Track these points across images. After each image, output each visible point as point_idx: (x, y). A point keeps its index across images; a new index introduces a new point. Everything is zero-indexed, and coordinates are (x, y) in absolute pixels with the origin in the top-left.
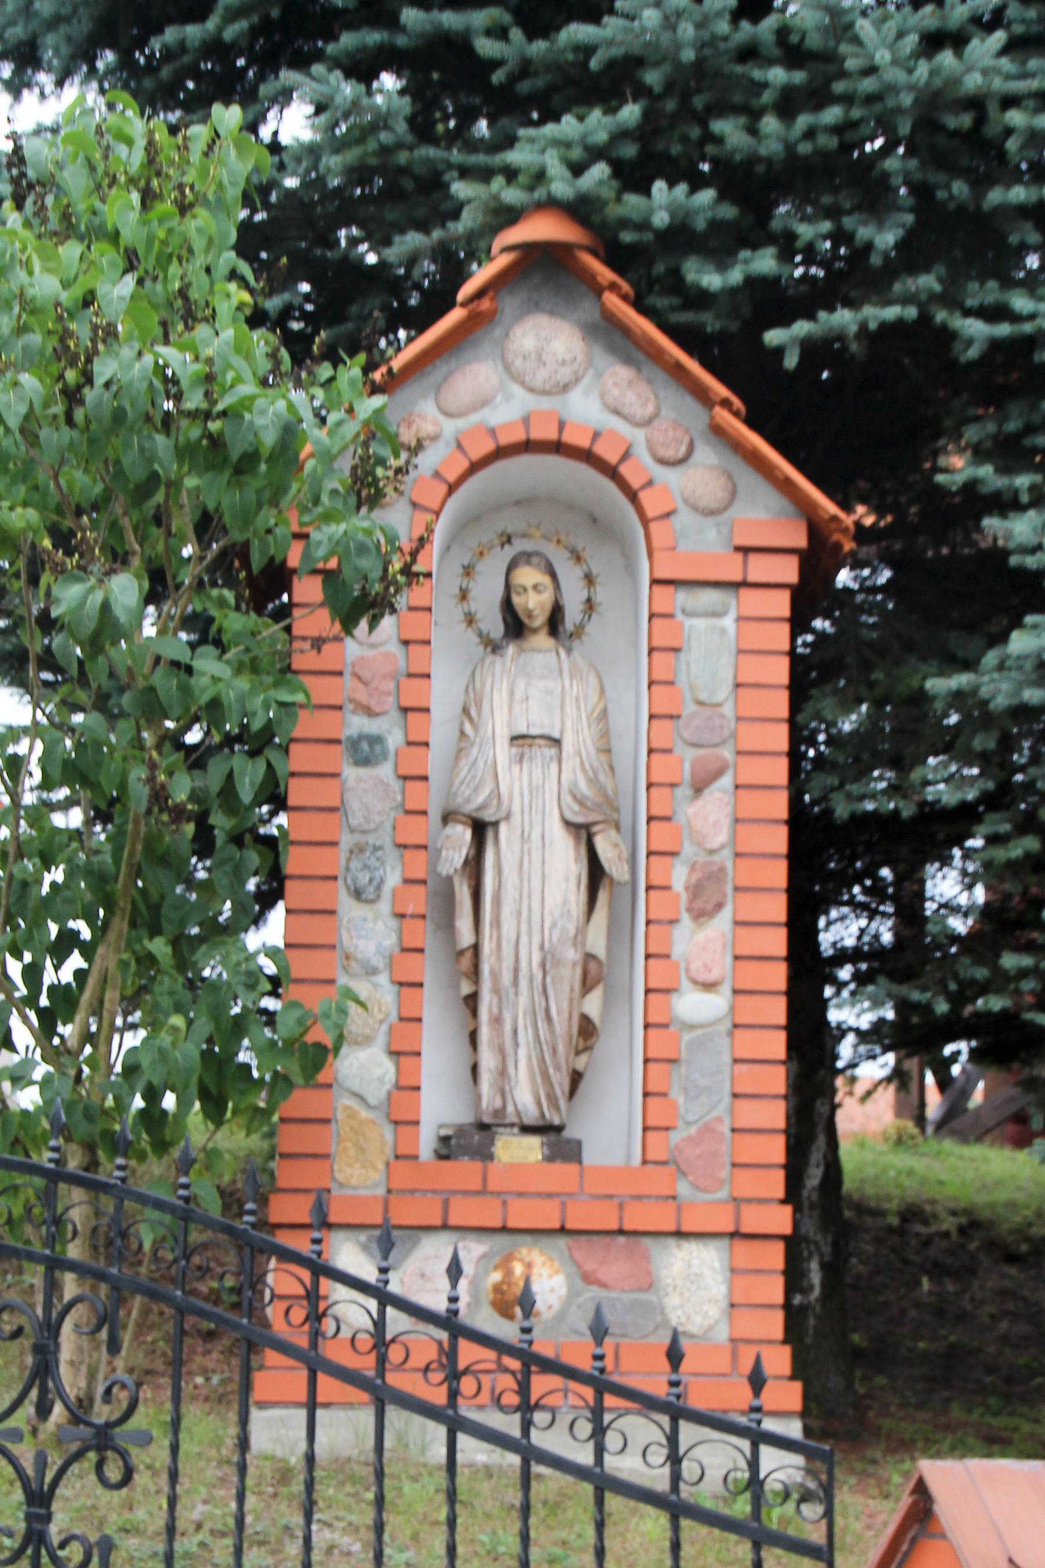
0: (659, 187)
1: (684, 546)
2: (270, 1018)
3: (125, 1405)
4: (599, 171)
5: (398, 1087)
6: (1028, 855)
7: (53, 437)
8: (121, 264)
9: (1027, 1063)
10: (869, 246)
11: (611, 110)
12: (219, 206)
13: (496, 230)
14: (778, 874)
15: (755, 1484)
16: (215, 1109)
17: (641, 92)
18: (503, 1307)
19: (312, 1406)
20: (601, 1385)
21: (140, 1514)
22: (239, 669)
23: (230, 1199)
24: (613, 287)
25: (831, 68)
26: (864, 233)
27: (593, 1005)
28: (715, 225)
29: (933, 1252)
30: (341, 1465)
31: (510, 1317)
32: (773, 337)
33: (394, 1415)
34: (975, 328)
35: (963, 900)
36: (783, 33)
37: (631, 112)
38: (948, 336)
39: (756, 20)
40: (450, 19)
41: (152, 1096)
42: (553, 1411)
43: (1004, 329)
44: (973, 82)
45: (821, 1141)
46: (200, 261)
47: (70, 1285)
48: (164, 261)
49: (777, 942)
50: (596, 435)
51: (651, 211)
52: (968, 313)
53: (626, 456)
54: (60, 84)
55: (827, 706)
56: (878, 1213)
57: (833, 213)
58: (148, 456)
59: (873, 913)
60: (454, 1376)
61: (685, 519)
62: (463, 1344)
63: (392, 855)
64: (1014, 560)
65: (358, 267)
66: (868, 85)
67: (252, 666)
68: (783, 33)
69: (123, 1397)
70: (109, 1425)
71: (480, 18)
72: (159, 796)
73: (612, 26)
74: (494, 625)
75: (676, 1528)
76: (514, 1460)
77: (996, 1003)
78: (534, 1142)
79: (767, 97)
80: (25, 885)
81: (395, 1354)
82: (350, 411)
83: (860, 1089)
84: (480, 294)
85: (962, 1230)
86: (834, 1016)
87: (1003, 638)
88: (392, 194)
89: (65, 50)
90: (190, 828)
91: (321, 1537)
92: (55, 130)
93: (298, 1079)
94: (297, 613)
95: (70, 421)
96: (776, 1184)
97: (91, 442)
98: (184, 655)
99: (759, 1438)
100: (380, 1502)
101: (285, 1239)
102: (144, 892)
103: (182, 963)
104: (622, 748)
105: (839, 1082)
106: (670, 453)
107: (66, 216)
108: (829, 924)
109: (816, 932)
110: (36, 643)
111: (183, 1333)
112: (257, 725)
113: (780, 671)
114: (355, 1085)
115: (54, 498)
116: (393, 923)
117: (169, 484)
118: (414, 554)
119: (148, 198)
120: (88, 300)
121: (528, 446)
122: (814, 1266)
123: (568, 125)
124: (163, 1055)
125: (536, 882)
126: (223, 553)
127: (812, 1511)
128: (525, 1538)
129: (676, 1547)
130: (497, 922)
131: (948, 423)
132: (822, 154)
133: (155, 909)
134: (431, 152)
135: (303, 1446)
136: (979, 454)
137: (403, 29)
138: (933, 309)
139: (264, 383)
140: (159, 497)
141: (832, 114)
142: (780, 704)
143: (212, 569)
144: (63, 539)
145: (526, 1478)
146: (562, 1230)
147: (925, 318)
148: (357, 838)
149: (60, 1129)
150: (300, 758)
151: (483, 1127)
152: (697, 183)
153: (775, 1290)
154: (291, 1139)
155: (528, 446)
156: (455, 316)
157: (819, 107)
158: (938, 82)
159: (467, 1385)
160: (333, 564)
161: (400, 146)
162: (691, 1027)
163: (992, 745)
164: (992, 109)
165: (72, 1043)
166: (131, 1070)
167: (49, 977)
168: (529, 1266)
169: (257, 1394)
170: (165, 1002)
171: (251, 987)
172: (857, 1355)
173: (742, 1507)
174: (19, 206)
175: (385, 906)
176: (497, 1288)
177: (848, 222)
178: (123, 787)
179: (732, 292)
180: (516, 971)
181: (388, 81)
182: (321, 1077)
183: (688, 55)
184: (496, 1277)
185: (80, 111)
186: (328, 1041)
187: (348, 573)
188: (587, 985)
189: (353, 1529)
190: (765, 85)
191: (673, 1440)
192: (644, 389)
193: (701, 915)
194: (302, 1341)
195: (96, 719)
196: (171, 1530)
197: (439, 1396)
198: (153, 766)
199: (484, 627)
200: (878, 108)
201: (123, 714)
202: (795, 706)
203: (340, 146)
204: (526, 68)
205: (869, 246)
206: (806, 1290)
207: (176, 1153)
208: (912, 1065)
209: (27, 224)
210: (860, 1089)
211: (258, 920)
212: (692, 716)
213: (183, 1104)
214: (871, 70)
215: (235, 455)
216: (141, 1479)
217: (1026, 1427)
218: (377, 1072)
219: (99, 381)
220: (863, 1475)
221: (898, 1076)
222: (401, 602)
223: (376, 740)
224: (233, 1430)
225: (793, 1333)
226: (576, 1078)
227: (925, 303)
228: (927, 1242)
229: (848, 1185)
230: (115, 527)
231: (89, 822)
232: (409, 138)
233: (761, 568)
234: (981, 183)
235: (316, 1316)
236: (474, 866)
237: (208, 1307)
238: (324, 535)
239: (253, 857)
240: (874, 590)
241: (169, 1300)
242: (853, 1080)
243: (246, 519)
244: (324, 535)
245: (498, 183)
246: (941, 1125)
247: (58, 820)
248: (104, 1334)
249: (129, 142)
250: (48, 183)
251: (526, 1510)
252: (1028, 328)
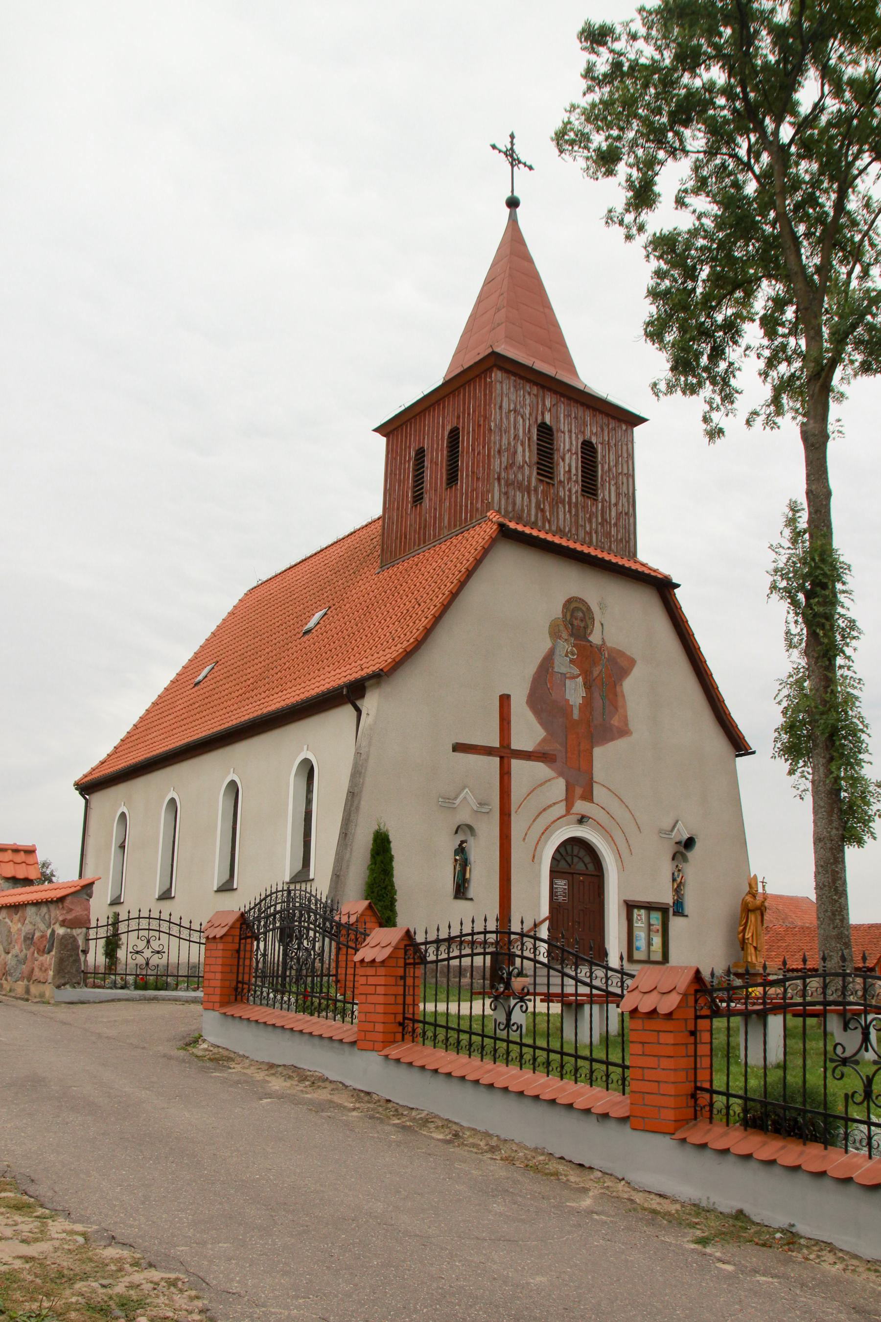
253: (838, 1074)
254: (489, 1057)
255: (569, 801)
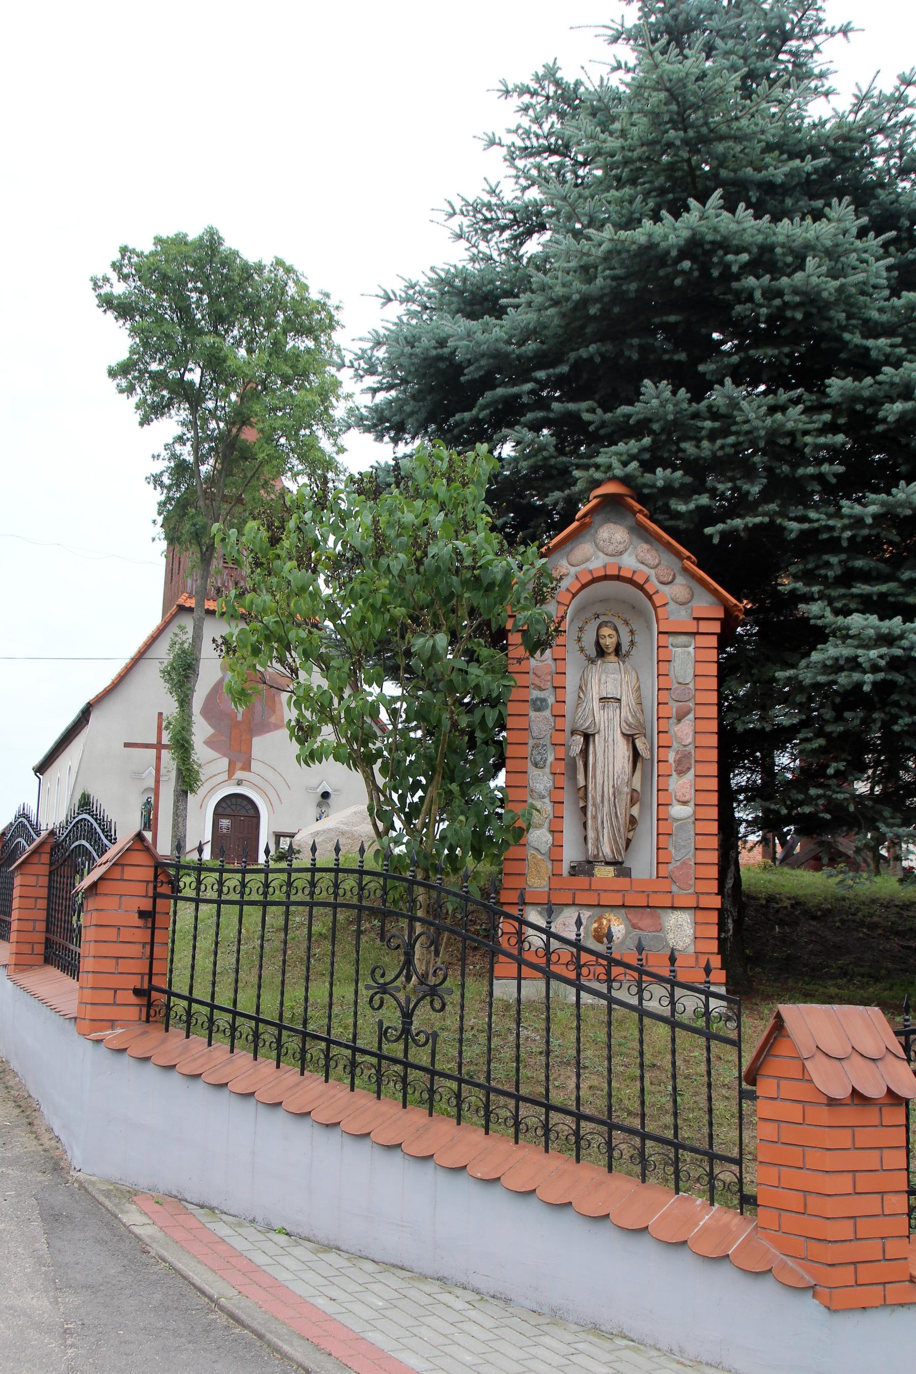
0: (659, 470)
1: (672, 618)
2: (500, 816)
3: (441, 977)
4: (634, 465)
5: (553, 845)
6: (820, 746)
7: (411, 578)
8: (439, 508)
9: (820, 835)
10: (748, 493)
11: (639, 440)
12: (478, 483)
13: (591, 490)
14: (714, 755)
15: (707, 1013)
16: (477, 856)
17: (651, 432)
18: (598, 938)
19: (519, 979)
20: (641, 972)
21: (448, 1022)
22: (487, 672)
23: (485, 893)
24: (640, 511)
25: (730, 421)
26: (746, 487)
27: (635, 811)
28: (683, 485)
29: (780, 915)
30: (531, 1003)
31: (602, 943)
32: (708, 530)
33: (554, 983)
34: (794, 525)
35: (792, 765)
36: (710, 407)
37: (647, 441)
38: (782, 529)
39: (698, 403)
40: (571, 406)
41: (452, 849)
42: (621, 982)
43: (806, 526)
44: (790, 425)
45: (733, 868)
46: (471, 506)
47: (419, 928)
48: (456, 506)
49: (713, 784)
50: (634, 572)
51: (656, 480)
52: (790, 519)
53: (647, 581)
54: (413, 438)
55: (733, 684)
56: (756, 898)
57: (732, 479)
58: (448, 584)
59: (753, 772)
60: (579, 967)
61: (672, 606)
62: (582, 954)
63: (550, 748)
64: (812, 622)
65: (533, 506)
66: (746, 427)
67: (491, 671)
68: (710, 407)
69: (440, 973)
70: (435, 986)
71: (584, 405)
72: (455, 725)
73: (639, 406)
74: (592, 651)
75: (673, 1032)
76: (605, 1002)
77: (807, 810)
78: (611, 868)
79: (704, 433)
80: (399, 762)
81: (554, 958)
82: (532, 564)
83: (748, 845)
84: (585, 516)
85: (792, 906)
86: (737, 815)
87: (808, 655)
88: (548, 476)
89: (415, 425)
90: (466, 738)
91: (524, 1033)
92: (411, 456)
93: (512, 842)
94: (510, 648)
95: (418, 572)
96: (714, 886)
97: (427, 580)
98: (464, 666)
99: (709, 994)
100: (548, 1019)
101: (507, 909)
102: (447, 764)
103: (463, 794)
104: (647, 703)
105: (740, 843)
106: (665, 579)
107: (417, 490)
108: (735, 776)
109: (730, 779)
110: (402, 662)
111: (465, 948)
112: (494, 695)
113: (713, 669)
114: (535, 844)
115: (412, 604)
116: (551, 777)
117: (458, 596)
118: (559, 623)
119: (450, 480)
120: (426, 523)
121: (606, 578)
122: (730, 921)
123: (621, 447)
124: (456, 832)
125: (611, 759)
126: (480, 625)
127: (732, 1025)
128: (609, 1036)
129: (673, 1040)
130: (594, 776)
131: (782, 565)
132: (726, 455)
133: (452, 771)
134: (564, 459)
135: (516, 995)
136: (796, 577)
137: (552, 411)
138: (775, 518)
139: (497, 554)
140: (454, 602)
141: (731, 440)
142: (713, 683)
143: (474, 631)
144: (415, 620)
145: (610, 1010)
146: (623, 906)
147: (772, 522)
148: (536, 741)
149: (415, 863)
150: (512, 708)
151: (589, 862)
152: (675, 469)
153: (714, 931)
154: (509, 867)
155: (606, 578)
156: (575, 524)
157: (726, 437)
158: (775, 426)
159: (584, 971)
160: (525, 628)
161: (552, 457)
162: (678, 820)
163: (804, 700)
164: (799, 436)
165: (418, 827)
166: (443, 838)
167: (409, 800)
168: (609, 921)
169: (495, 974)
170: (457, 810)
171: (493, 804)
172: (748, 958)
173: (701, 1023)
174: (398, 487)
175: (547, 770)
176: (596, 930)
177: (739, 483)
178: (439, 721)
179: (690, 512)
180: (603, 796)
181: (545, 431)
182: (521, 842)
183: (671, 417)
184: (596, 925)
185: (422, 447)
186: (524, 826)
187: (532, 631)
188: (633, 802)
189: (536, 1030)
190: (703, 428)
191: (672, 995)
192: (654, 553)
193: (681, 772)
194: (515, 952)
195: (428, 693)
196: (461, 1029)
197: (572, 975)
198: (452, 712)
199: (588, 653)
200: (750, 436)
201: (438, 691)
202: (720, 684)
203: (527, 457)
204: (603, 424)
205: (748, 493)
206: (727, 932)
207: (462, 873)
208: (770, 835)
209: (401, 493)
210: (748, 845)
211: (494, 776)
212: (676, 689)
213: (464, 853)
214: (747, 421)
215: (485, 584)
216: (448, 1008)
217: (821, 990)
218: (545, 839)
219: (430, 555)
220: (752, 1010)
221: (764, 841)
222: (554, 643)
223: (543, 700)
224: (486, 988)
225: (721, 950)
226: (628, 842)
227: (772, 515)
228: (778, 911)
229: (744, 887)
230: (435, 615)
231: (424, 736)
232: (555, 454)
233: (704, 627)
234: (794, 466)
235: (521, 942)
236: (585, 752)
237: (475, 937)
238: (522, 616)
239: (493, 750)
240: (752, 635)
241: (460, 934)
242: (746, 842)
243: (490, 610)
244: (522, 616)
245: (592, 470)
246: (783, 861)
247: (412, 735)
248: (433, 948)
249: (442, 459)
250: (409, 477)
251: (609, 1024)
252: (816, 525)
253: (376, 1003)
254: (242, 1041)
255: (231, 772)
